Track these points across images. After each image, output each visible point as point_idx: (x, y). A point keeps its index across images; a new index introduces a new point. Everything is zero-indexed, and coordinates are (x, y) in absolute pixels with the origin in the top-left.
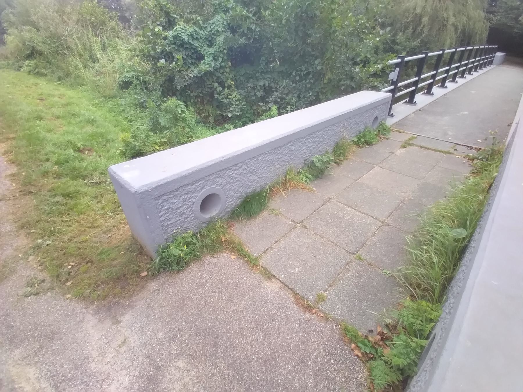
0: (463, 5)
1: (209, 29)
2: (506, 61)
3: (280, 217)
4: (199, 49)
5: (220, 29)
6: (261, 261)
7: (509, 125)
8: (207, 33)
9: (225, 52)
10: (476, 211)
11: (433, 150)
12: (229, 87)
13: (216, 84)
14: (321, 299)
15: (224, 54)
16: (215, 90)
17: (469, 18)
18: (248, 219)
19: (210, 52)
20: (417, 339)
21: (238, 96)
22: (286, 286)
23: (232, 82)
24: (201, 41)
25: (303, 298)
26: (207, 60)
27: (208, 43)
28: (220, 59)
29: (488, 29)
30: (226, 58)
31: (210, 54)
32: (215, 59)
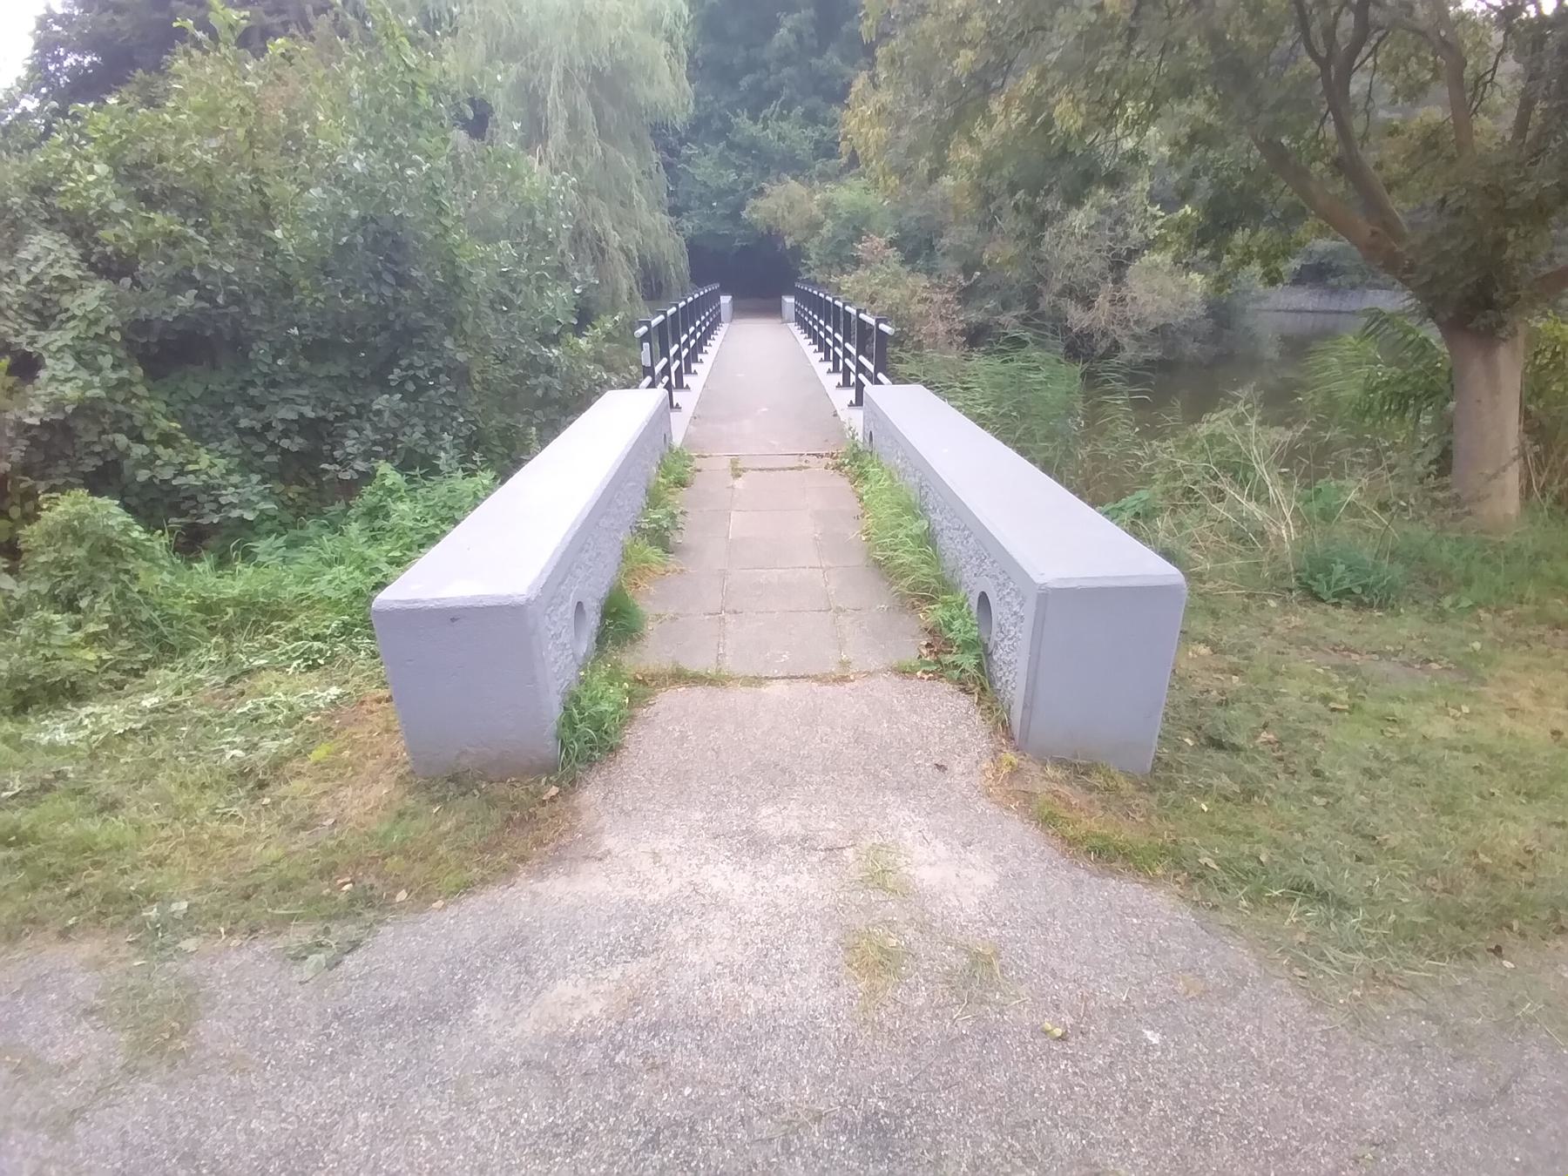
0: (622, 204)
1: (26, 278)
2: (740, 311)
3: (681, 619)
4: (13, 340)
5: (68, 272)
6: (724, 672)
7: (835, 415)
8: (23, 289)
9: (116, 336)
10: (516, 1060)
11: (780, 469)
12: (167, 440)
13: (122, 440)
14: (845, 664)
15: (113, 343)
16: (125, 454)
17: (645, 232)
18: (633, 641)
19: (60, 344)
20: (1047, 239)
21: (221, 463)
22: (792, 677)
23: (174, 425)
24: (10, 313)
25: (825, 676)
26: (53, 367)
27: (33, 318)
28: (106, 361)
29: (685, 250)
30: (121, 353)
31: (60, 350)
32: (84, 358)
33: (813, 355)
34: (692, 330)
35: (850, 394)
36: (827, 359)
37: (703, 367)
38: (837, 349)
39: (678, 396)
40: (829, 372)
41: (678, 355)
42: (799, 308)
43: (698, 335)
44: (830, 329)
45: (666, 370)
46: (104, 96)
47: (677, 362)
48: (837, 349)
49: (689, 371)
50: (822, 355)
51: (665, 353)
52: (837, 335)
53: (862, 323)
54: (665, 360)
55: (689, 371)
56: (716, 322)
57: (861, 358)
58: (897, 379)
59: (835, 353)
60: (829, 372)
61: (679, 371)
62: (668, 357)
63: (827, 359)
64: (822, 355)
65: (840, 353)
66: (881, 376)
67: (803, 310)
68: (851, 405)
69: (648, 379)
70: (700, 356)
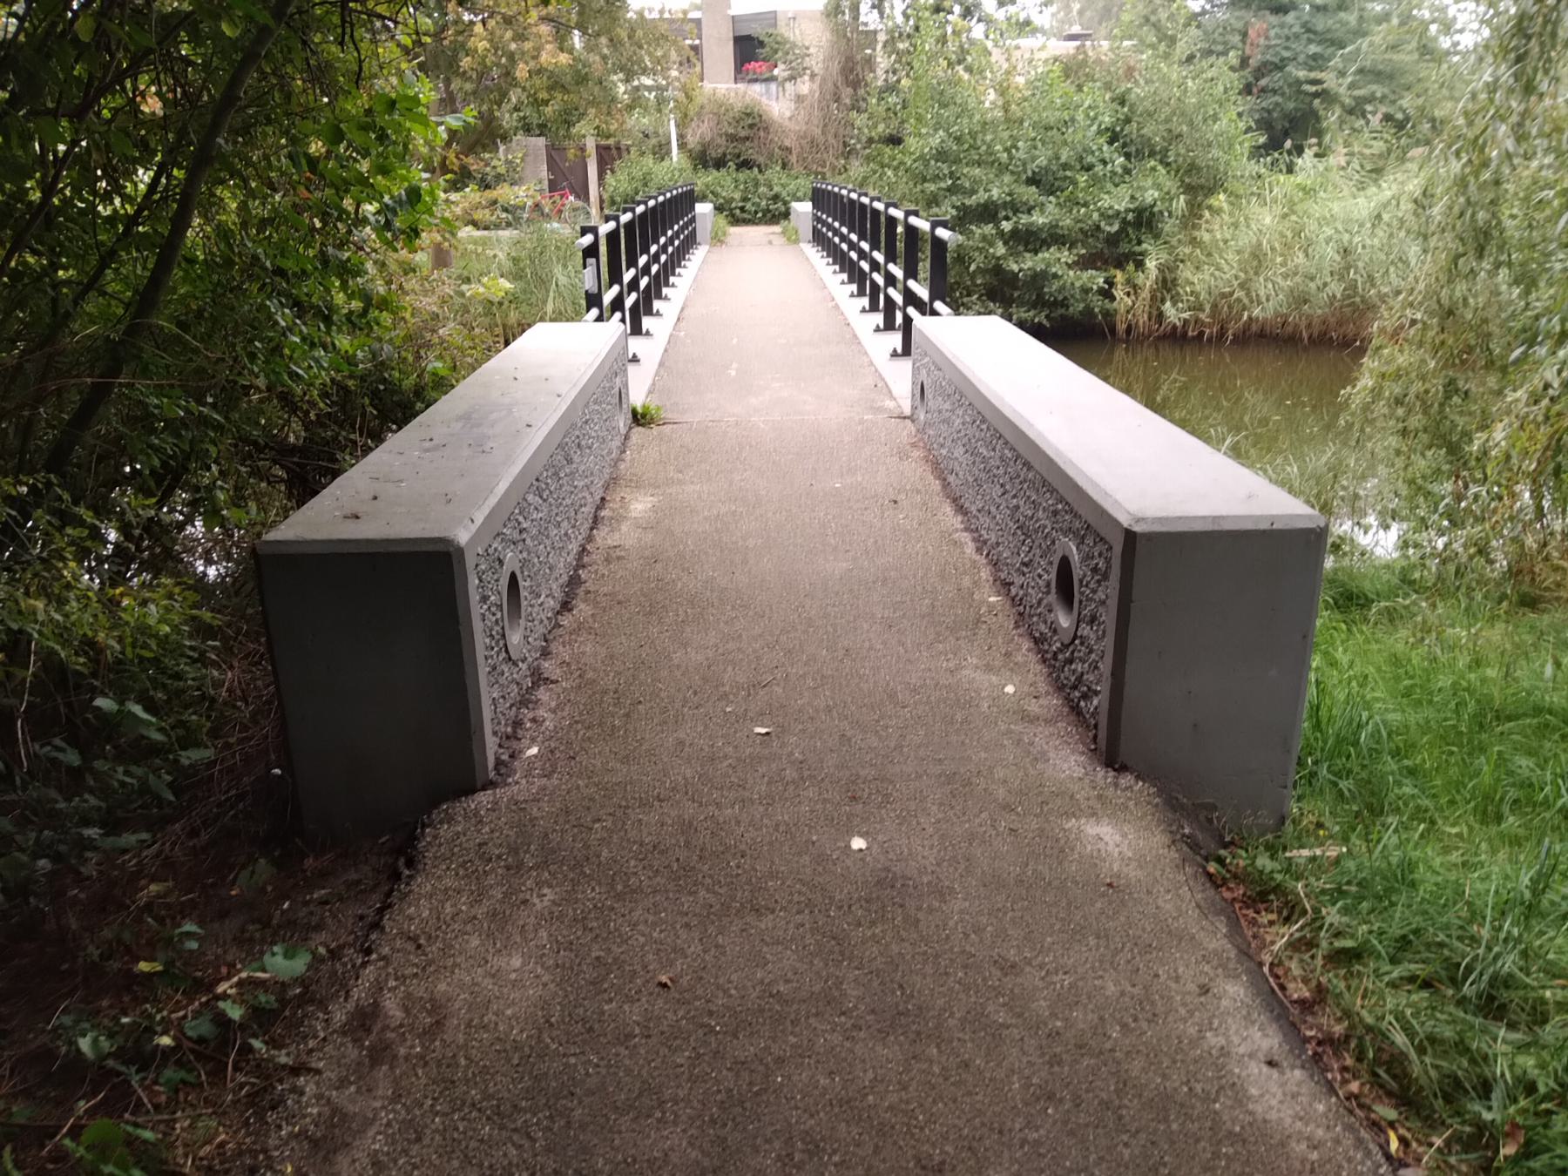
33: (852, 304)
34: (654, 249)
35: (895, 340)
36: (874, 307)
37: (668, 307)
38: (891, 291)
39: (636, 345)
40: (877, 330)
41: (634, 285)
42: (818, 220)
43: (663, 258)
44: (879, 257)
45: (617, 304)
46: (1564, 200)
47: (634, 296)
48: (891, 291)
49: (649, 312)
50: (854, 287)
51: (615, 277)
52: (892, 267)
53: (911, 231)
54: (616, 289)
55: (649, 312)
56: (690, 242)
57: (911, 284)
58: (958, 308)
59: (888, 298)
60: (877, 330)
61: (635, 309)
62: (621, 284)
63: (874, 307)
64: (854, 287)
65: (898, 298)
66: (938, 305)
67: (824, 223)
68: (895, 354)
69: (594, 312)
70: (665, 291)
